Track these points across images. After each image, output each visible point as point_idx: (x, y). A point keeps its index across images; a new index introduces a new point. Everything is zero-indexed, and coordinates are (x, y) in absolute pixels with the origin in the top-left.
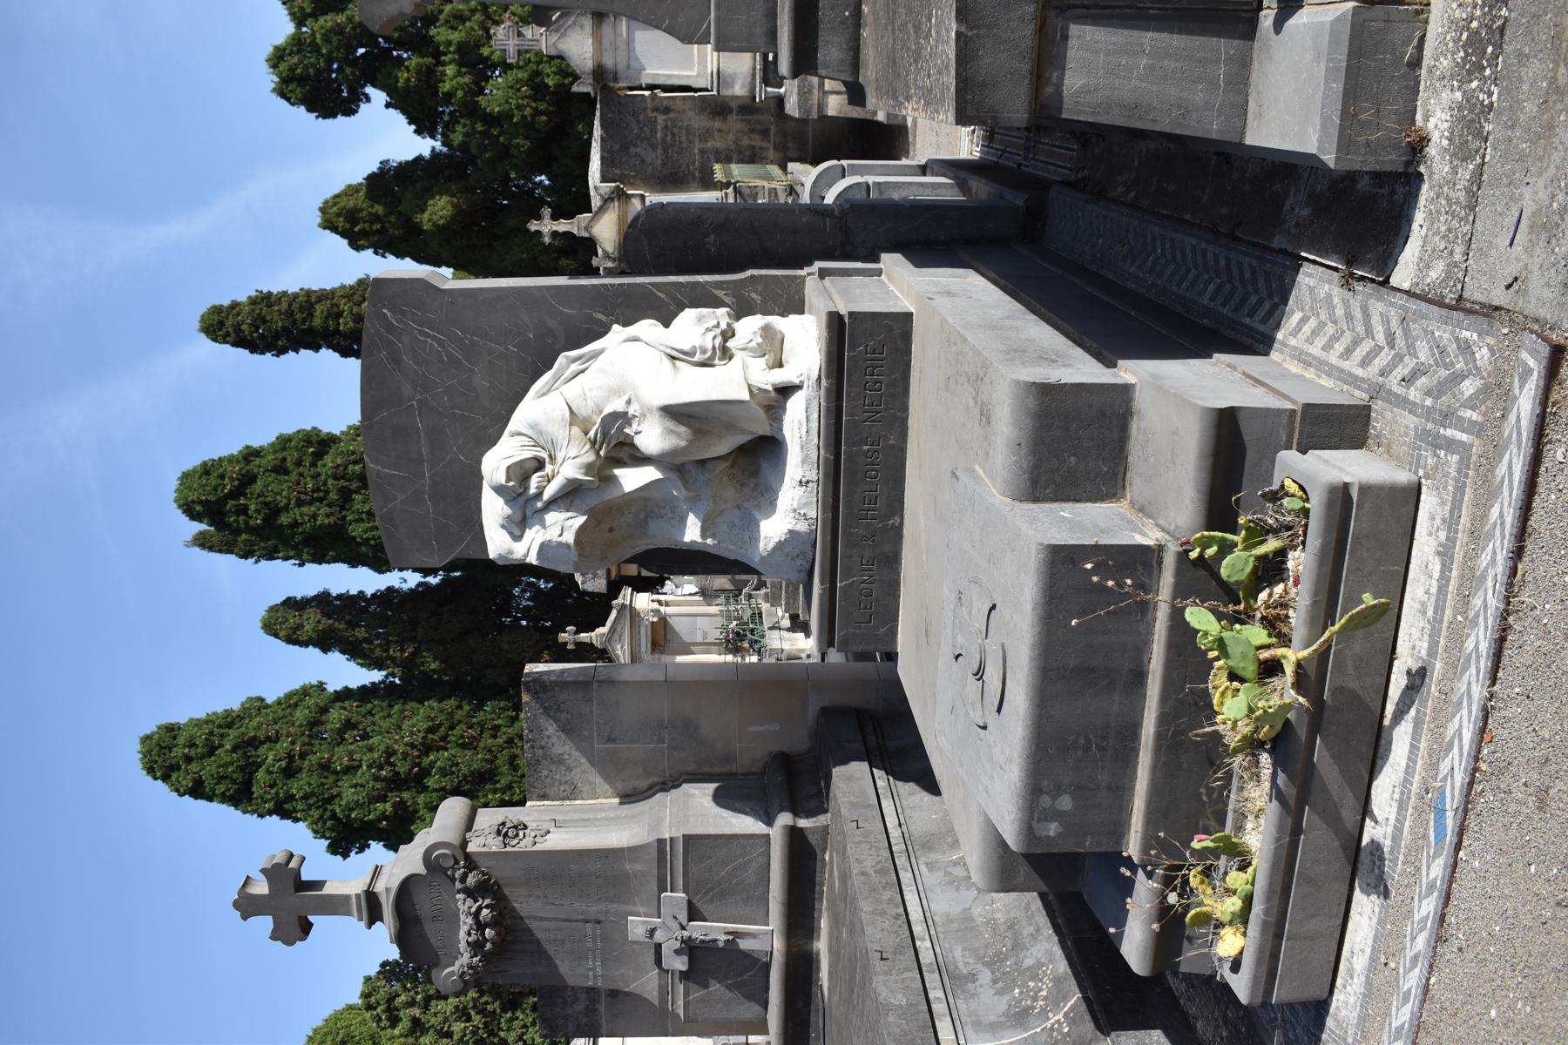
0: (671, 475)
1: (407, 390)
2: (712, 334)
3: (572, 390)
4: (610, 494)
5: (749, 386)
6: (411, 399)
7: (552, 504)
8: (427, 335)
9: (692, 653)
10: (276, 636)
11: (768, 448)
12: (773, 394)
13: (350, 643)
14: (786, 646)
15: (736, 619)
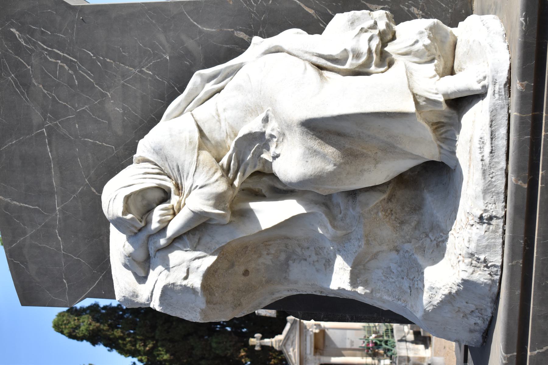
0: (316, 209)
1: (37, 117)
2: (368, 35)
3: (204, 113)
4: (244, 231)
5: (415, 96)
6: (40, 126)
7: (176, 241)
8: (57, 57)
9: (342, 355)
10: (62, 332)
11: (437, 176)
12: (444, 107)
13: (110, 339)
14: (411, 355)
15: (375, 332)
